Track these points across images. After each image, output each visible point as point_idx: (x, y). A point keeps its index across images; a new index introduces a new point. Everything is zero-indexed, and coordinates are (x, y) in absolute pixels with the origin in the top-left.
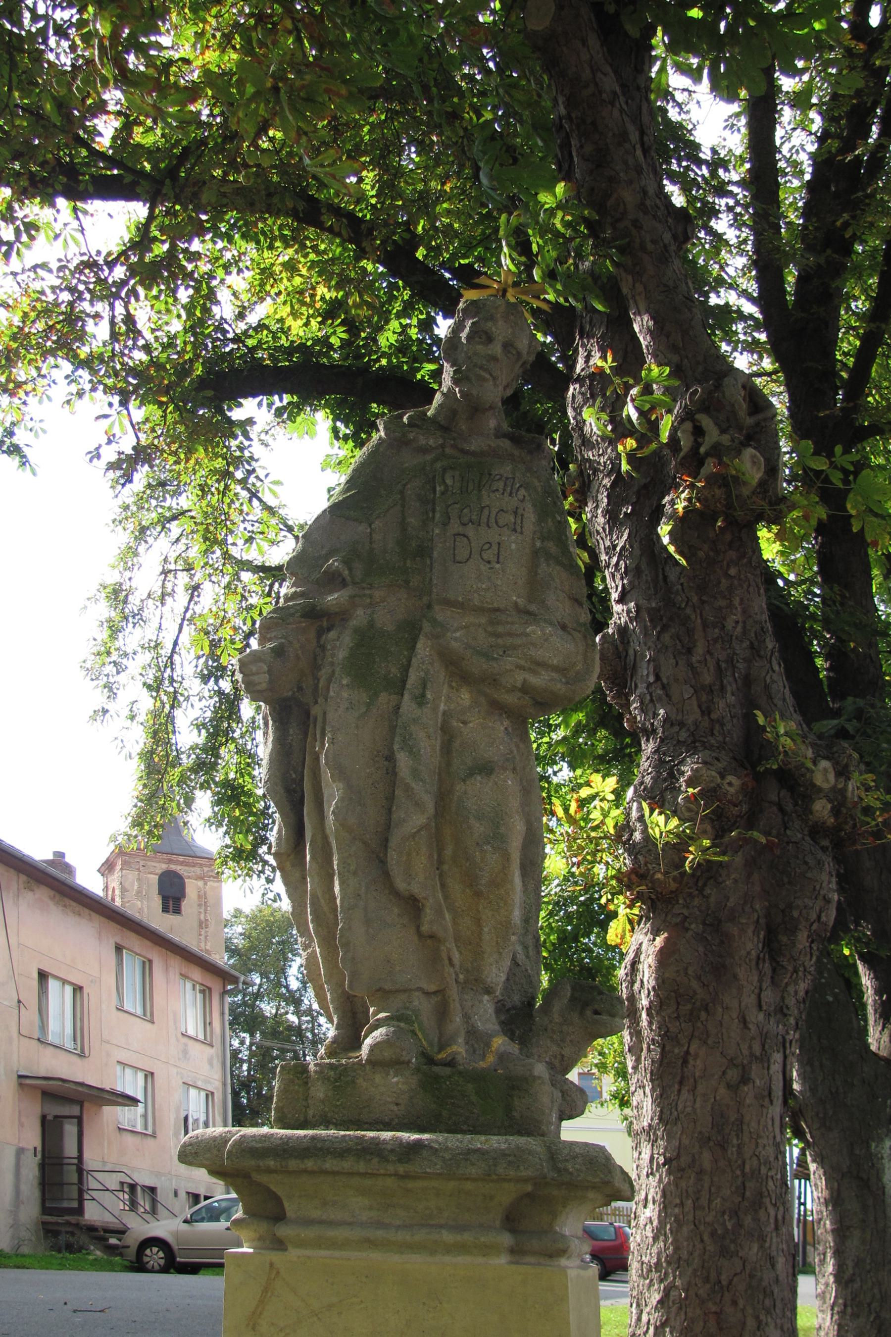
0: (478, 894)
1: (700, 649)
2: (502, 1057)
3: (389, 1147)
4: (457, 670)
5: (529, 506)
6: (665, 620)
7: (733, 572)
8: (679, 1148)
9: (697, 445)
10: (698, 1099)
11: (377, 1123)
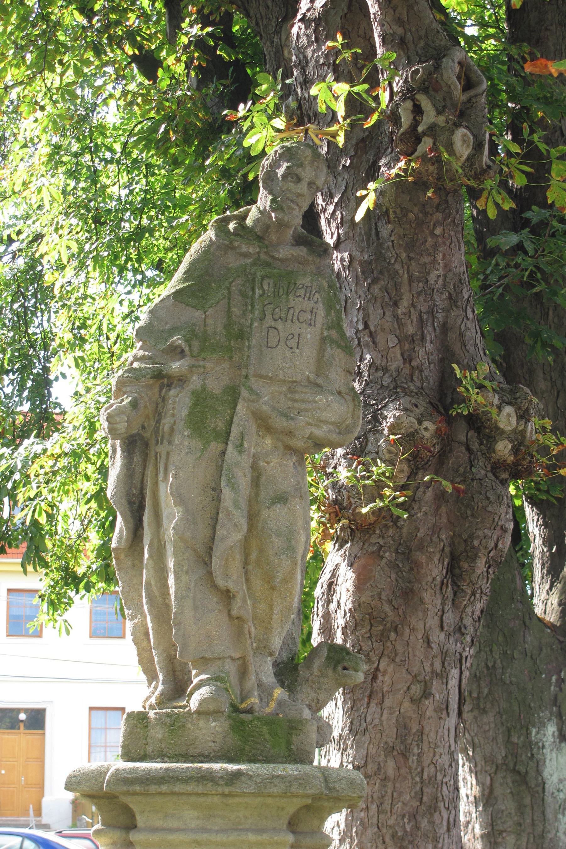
0: (273, 588)
1: (405, 303)
2: (280, 704)
3: (219, 775)
4: (264, 425)
5: (320, 305)
6: (376, 274)
7: (438, 231)
8: (367, 756)
9: (415, 124)
10: (385, 712)
11: (199, 756)
